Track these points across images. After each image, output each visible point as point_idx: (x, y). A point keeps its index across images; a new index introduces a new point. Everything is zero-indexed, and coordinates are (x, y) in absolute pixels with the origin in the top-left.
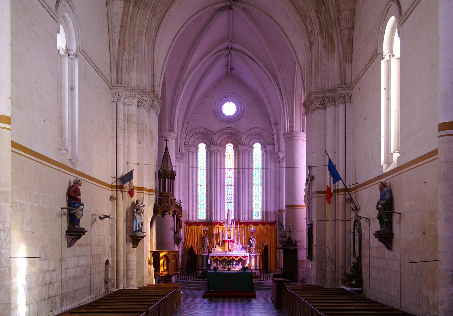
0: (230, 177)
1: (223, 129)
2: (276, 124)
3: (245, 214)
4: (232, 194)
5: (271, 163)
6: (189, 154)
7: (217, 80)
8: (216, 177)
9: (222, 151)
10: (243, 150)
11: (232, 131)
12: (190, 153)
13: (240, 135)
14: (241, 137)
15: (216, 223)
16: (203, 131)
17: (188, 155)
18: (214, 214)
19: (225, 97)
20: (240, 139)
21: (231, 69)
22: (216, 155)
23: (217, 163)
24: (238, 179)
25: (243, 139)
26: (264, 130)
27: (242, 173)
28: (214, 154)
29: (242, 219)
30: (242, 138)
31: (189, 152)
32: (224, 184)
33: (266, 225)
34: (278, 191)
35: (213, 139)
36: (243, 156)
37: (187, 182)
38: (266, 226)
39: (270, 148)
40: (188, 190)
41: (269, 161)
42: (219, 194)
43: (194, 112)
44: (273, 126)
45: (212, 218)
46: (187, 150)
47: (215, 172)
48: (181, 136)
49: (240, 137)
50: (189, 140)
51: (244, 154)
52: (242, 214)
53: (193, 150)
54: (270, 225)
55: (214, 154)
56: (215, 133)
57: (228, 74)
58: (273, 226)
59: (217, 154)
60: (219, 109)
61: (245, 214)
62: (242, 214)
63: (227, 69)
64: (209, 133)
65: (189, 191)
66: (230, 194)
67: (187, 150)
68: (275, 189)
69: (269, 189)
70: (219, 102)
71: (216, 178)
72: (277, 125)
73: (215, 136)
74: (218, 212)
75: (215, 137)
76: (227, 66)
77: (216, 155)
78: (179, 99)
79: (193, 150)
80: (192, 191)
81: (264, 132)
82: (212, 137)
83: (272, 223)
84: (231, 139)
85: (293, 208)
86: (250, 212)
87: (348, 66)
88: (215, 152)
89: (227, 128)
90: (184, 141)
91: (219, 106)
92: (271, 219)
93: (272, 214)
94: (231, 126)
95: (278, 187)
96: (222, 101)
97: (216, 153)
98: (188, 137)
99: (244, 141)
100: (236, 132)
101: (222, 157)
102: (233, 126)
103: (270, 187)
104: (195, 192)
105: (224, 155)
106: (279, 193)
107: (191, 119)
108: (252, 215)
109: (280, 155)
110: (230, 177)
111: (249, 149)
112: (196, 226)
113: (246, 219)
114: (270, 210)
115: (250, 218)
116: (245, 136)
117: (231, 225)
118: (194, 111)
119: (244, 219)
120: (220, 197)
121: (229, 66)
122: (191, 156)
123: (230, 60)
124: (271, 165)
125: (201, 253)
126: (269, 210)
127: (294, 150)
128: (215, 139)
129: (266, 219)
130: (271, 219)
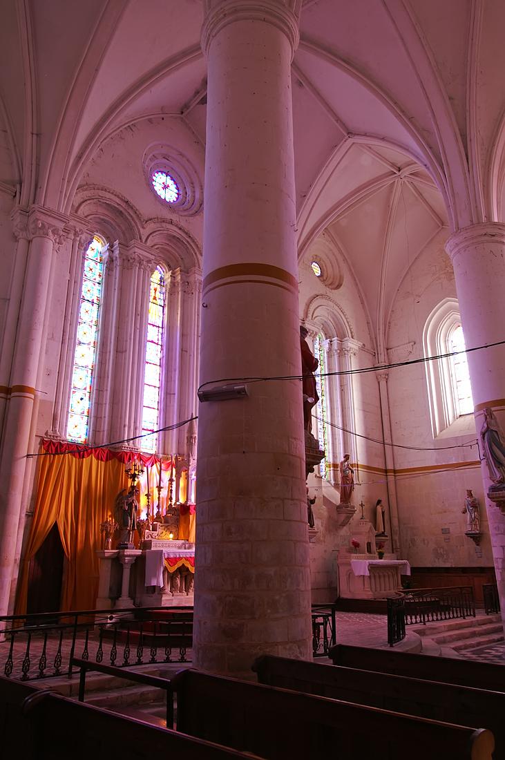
49: (196, 254)
52: (127, 429)
57: (182, 113)
59: (145, 270)
75: (143, 228)
84: (168, 251)
123: (195, 96)
128: (144, 233)
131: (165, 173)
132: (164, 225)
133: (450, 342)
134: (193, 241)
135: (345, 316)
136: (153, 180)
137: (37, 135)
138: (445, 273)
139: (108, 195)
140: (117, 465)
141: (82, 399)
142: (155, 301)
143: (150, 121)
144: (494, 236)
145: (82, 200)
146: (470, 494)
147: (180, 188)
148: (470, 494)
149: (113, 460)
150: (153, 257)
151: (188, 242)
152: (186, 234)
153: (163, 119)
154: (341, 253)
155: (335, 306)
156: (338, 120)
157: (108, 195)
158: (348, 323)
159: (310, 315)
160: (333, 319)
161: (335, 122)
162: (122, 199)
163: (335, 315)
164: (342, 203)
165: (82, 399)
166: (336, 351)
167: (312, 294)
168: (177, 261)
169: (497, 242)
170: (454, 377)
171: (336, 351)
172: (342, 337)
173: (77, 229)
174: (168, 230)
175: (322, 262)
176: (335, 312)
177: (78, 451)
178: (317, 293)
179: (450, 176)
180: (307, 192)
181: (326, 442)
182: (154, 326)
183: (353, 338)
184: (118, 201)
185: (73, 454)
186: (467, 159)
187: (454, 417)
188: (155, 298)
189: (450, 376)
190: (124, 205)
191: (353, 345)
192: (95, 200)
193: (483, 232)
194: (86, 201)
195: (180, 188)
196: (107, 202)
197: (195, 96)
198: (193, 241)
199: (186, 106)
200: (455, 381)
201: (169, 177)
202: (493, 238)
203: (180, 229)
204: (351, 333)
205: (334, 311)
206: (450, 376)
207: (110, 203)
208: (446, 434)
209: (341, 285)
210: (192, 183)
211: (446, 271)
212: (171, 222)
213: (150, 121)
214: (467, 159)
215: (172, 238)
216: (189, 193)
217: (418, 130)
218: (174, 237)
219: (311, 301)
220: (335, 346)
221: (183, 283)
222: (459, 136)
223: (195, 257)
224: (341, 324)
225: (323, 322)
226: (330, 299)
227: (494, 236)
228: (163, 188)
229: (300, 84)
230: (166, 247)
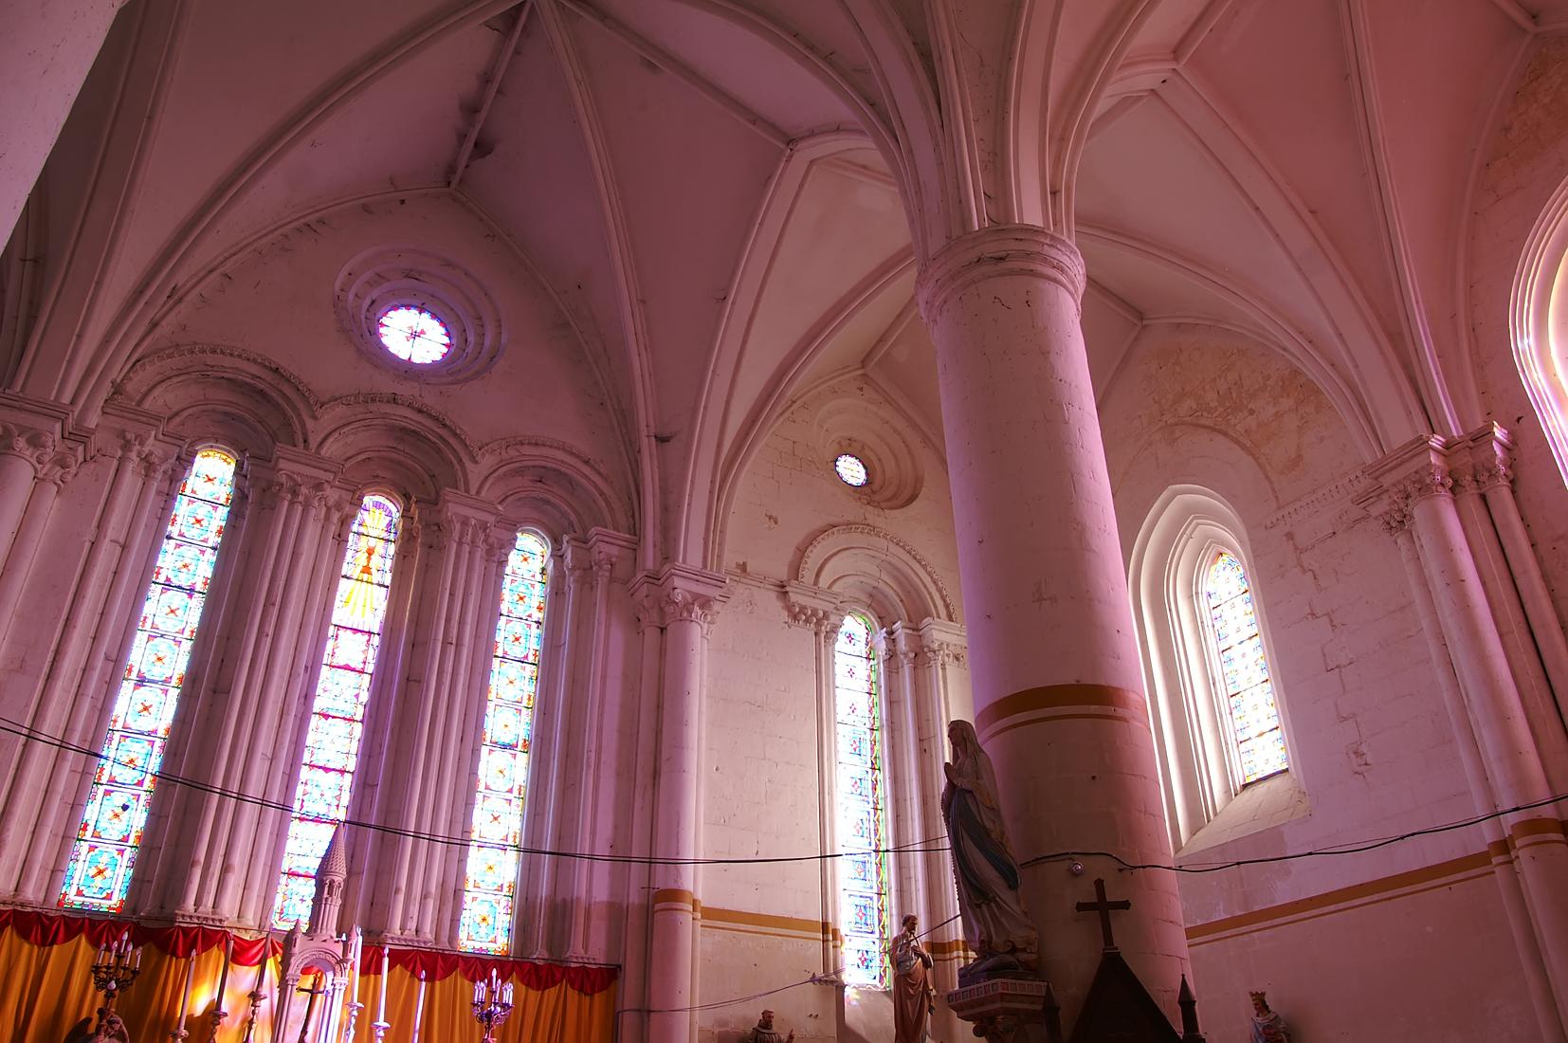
0: (347, 668)
2: (662, 439)
3: (425, 896)
4: (342, 772)
6: (122, 460)
8: (271, 632)
9: (338, 507)
10: (465, 523)
12: (133, 455)
13: (462, 454)
14: (466, 460)
15: (208, 937)
16: (254, 369)
17: (115, 463)
18: (197, 872)
20: (457, 467)
21: (483, 148)
23: (295, 555)
24: (408, 679)
25: (475, 472)
26: (587, 462)
27: (439, 644)
29: (403, 929)
30: (469, 465)
31: (127, 446)
32: (308, 696)
33: (554, 985)
34: (642, 777)
37: (57, 618)
38: (552, 993)
39: (614, 551)
40: (46, 669)
41: (600, 611)
42: (264, 745)
43: (227, 267)
44: (647, 445)
45: (180, 897)
46: (121, 434)
48: (106, 341)
49: (460, 460)
51: (466, 548)
52: (401, 897)
53: (159, 452)
54: (581, 990)
55: (292, 503)
57: (449, 184)
58: (597, 996)
60: (363, 317)
61: (425, 896)
62: (401, 897)
63: (462, 137)
65: (50, 677)
66: (330, 765)
67: (121, 434)
68: (626, 774)
69: (588, 766)
70: (369, 284)
72: (664, 444)
74: (239, 859)
75: (315, 418)
79: (159, 452)
80: (74, 690)
81: (586, 469)
82: (299, 415)
83: (602, 979)
84: (400, 463)
85: (1094, 709)
86: (452, 897)
87: (608, 627)
88: (295, 493)
90: (116, 374)
91: (368, 302)
92: (586, 948)
93: (594, 922)
95: (644, 761)
96: (386, 286)
97: (301, 498)
99: (477, 485)
102: (430, 400)
103: (593, 754)
104: (93, 707)
105: (341, 540)
106: (650, 792)
108: (455, 922)
109: (676, 584)
110: (347, 668)
112: (26, 947)
113: (428, 932)
114: (583, 895)
115: (444, 939)
116: (487, 461)
117: (339, 950)
118: (230, 263)
119: (410, 933)
120: (267, 763)
122: (130, 481)
123: (460, 144)
124: (611, 642)
126: (581, 891)
127: (1046, 328)
128: (316, 430)
129: (550, 950)
130: (590, 947)
132: (373, 407)
133: (1203, 598)
134: (455, 434)
136: (383, 325)
137: (35, 261)
139: (228, 362)
140: (406, 982)
141: (125, 808)
142: (365, 577)
146: (1260, 1003)
148: (1260, 1003)
149: (146, 946)
152: (437, 419)
153: (403, 202)
154: (914, 425)
156: (756, 119)
157: (228, 362)
160: (895, 578)
161: (751, 126)
163: (898, 569)
164: (847, 305)
165: (125, 808)
166: (906, 655)
167: (820, 522)
168: (423, 483)
169: (1012, 273)
170: (1220, 685)
171: (906, 655)
172: (917, 615)
173: (129, 436)
174: (384, 416)
176: (894, 561)
177: (478, 966)
178: (833, 520)
179: (911, 151)
180: (728, 289)
181: (885, 889)
183: (950, 619)
184: (254, 369)
185: (25, 934)
187: (1227, 791)
189: (1210, 683)
191: (947, 635)
192: (193, 376)
193: (973, 255)
197: (460, 144)
199: (451, 169)
200: (1223, 696)
203: (420, 411)
204: (947, 606)
205: (889, 558)
206: (1210, 683)
208: (1205, 840)
209: (917, 496)
211: (1161, 424)
212: (394, 400)
213: (366, 208)
215: (405, 433)
216: (471, 339)
219: (811, 540)
220: (902, 645)
221: (427, 525)
223: (457, 467)
224: (917, 590)
226: (873, 530)
229: (652, 67)
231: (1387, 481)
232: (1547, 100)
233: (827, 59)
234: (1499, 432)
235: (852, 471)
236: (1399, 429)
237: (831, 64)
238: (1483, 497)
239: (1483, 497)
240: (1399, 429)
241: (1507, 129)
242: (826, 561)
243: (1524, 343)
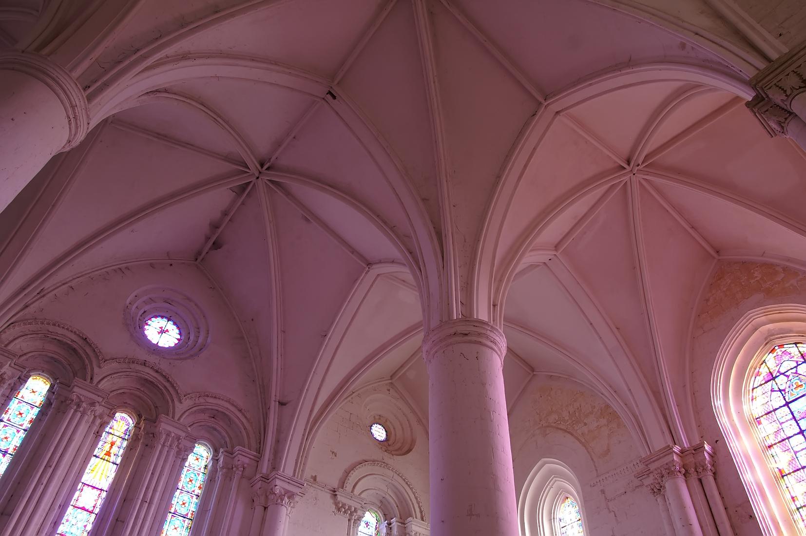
1: (133, 361)
2: (282, 404)
5: (236, 503)
7: (168, 253)
8: (45, 483)
10: (168, 435)
11: (155, 375)
13: (174, 396)
19: (165, 302)
21: (217, 245)
22: (79, 414)
23: (70, 440)
25: (180, 408)
26: (240, 411)
27: (140, 501)
28: (72, 411)
35: (92, 369)
36: (161, 452)
39: (247, 460)
44: (274, 406)
47: (48, 466)
49: (173, 401)
50: (15, 339)
51: (166, 449)
55: (76, 411)
56: (107, 358)
57: (197, 259)
59: (83, 414)
63: (208, 238)
64: (88, 350)
71: (43, 487)
73: (102, 365)
75: (100, 367)
76: (215, 226)
77: (79, 414)
78: (62, 193)
88: (79, 406)
89: (144, 364)
94: (157, 361)
97: (81, 409)
98: (17, 330)
100: (167, 384)
101: (92, 435)
102: (164, 366)
107: (53, 293)
111: (185, 443)
116: (187, 403)
121: (220, 230)
125: (781, 280)
128: (99, 373)
131: (166, 318)
132: (133, 366)
134: (173, 386)
135: (411, 489)
138: (539, 428)
139: (60, 331)
143: (152, 265)
144: (466, 335)
145: (21, 334)
147: (183, 333)
150: (100, 399)
151: (165, 387)
152: (165, 377)
153: (171, 265)
154: (414, 412)
155: (396, 476)
156: (353, 251)
157: (60, 331)
158: (416, 498)
159: (349, 486)
161: (351, 254)
162: (78, 335)
169: (470, 342)
175: (388, 423)
182: (94, 488)
183: (422, 519)
184: (74, 337)
186: (443, 257)
188: (108, 454)
190: (80, 342)
193: (452, 331)
194: (27, 335)
195: (183, 333)
196: (58, 338)
198: (173, 386)
199: (199, 253)
201: (170, 322)
202: (466, 338)
203: (157, 372)
204: (421, 512)
207: (60, 339)
210: (787, 487)
212: (144, 364)
213: (152, 265)
214: (443, 257)
215: (147, 383)
216: (192, 338)
217: (398, 237)
218: (146, 380)
219: (353, 468)
221: (147, 433)
222: (434, 234)
224: (406, 501)
225: (381, 498)
226: (387, 465)
227: (466, 335)
228: (159, 333)
229: (307, 220)
230: (138, 393)
231: (652, 467)
232: (725, 289)
233: (392, 228)
234: (707, 447)
235: (379, 432)
236: (659, 441)
237: (393, 231)
238: (700, 480)
239: (700, 480)
240: (659, 441)
241: (707, 300)
242: (360, 480)
243: (718, 403)
